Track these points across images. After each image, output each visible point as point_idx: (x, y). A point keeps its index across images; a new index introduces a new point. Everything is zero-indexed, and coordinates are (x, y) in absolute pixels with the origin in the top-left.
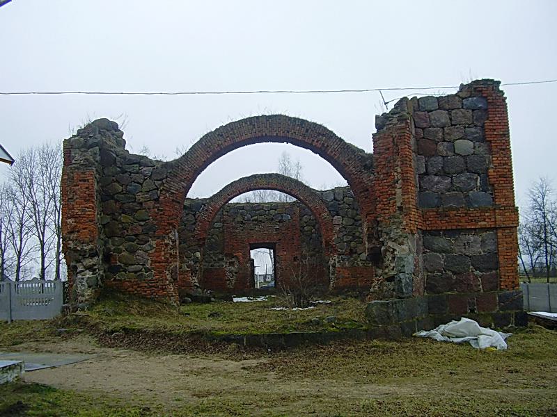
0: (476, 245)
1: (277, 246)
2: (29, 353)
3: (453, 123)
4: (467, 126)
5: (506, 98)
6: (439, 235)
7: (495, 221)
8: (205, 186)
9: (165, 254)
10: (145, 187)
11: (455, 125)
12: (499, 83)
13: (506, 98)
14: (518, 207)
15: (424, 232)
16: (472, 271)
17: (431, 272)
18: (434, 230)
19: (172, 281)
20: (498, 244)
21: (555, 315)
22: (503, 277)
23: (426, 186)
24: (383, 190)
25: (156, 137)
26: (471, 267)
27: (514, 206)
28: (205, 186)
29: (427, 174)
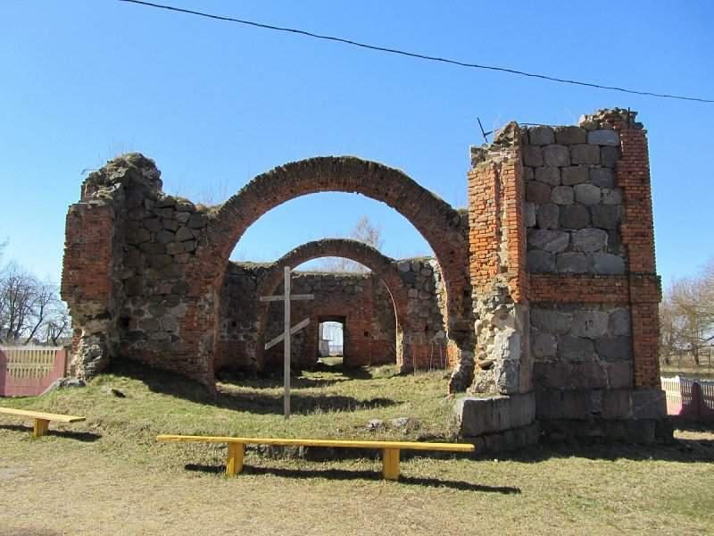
0: (600, 322)
1: (347, 320)
2: (29, 278)
3: (574, 162)
4: (592, 166)
5: (646, 131)
6: (552, 309)
7: (629, 294)
8: (259, 245)
9: (199, 319)
10: (179, 236)
11: (577, 165)
12: (635, 113)
13: (646, 131)
14: (660, 277)
15: (532, 305)
16: (596, 361)
17: (539, 358)
18: (545, 302)
19: (207, 353)
20: (631, 325)
21: (708, 436)
22: (638, 370)
23: (537, 243)
24: (480, 244)
25: (198, 179)
26: (594, 354)
27: (655, 274)
28: (259, 245)
29: (537, 227)
